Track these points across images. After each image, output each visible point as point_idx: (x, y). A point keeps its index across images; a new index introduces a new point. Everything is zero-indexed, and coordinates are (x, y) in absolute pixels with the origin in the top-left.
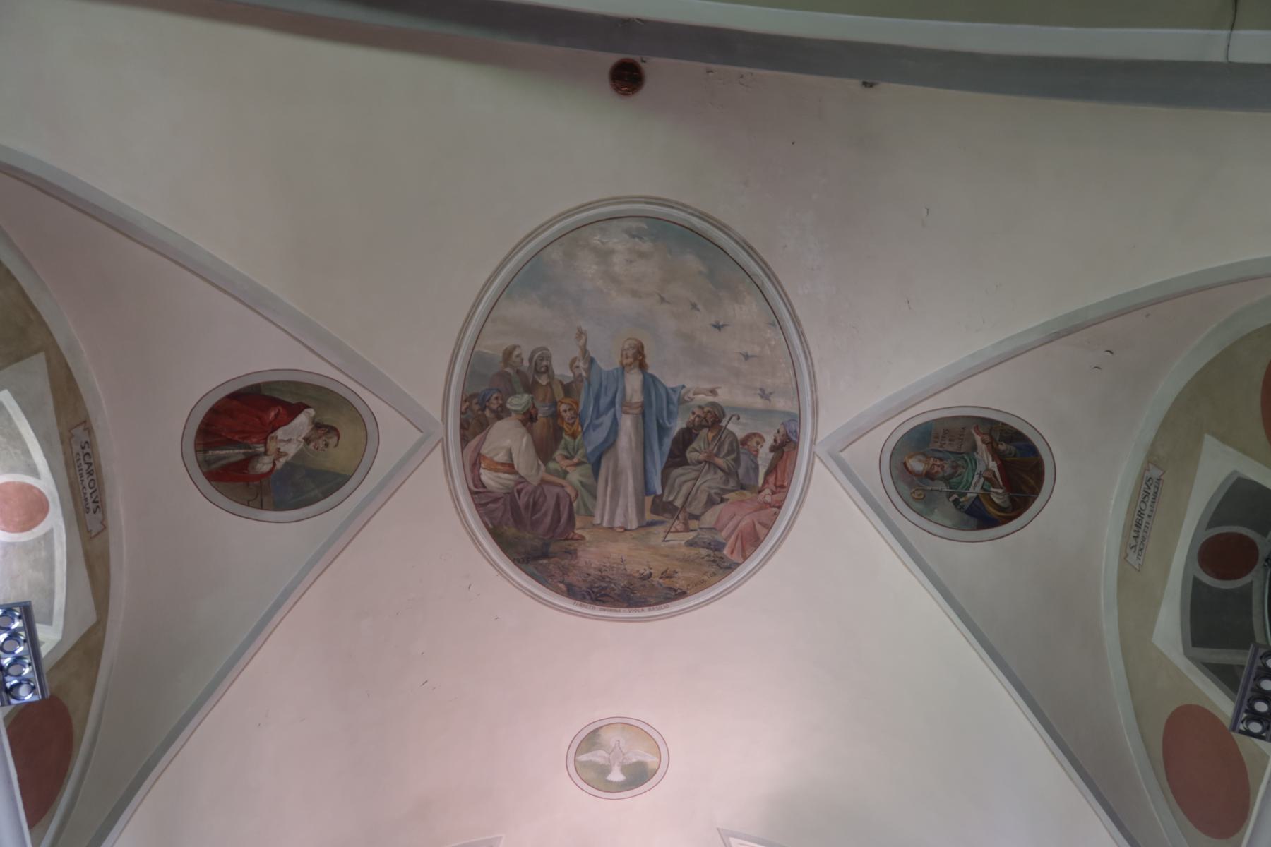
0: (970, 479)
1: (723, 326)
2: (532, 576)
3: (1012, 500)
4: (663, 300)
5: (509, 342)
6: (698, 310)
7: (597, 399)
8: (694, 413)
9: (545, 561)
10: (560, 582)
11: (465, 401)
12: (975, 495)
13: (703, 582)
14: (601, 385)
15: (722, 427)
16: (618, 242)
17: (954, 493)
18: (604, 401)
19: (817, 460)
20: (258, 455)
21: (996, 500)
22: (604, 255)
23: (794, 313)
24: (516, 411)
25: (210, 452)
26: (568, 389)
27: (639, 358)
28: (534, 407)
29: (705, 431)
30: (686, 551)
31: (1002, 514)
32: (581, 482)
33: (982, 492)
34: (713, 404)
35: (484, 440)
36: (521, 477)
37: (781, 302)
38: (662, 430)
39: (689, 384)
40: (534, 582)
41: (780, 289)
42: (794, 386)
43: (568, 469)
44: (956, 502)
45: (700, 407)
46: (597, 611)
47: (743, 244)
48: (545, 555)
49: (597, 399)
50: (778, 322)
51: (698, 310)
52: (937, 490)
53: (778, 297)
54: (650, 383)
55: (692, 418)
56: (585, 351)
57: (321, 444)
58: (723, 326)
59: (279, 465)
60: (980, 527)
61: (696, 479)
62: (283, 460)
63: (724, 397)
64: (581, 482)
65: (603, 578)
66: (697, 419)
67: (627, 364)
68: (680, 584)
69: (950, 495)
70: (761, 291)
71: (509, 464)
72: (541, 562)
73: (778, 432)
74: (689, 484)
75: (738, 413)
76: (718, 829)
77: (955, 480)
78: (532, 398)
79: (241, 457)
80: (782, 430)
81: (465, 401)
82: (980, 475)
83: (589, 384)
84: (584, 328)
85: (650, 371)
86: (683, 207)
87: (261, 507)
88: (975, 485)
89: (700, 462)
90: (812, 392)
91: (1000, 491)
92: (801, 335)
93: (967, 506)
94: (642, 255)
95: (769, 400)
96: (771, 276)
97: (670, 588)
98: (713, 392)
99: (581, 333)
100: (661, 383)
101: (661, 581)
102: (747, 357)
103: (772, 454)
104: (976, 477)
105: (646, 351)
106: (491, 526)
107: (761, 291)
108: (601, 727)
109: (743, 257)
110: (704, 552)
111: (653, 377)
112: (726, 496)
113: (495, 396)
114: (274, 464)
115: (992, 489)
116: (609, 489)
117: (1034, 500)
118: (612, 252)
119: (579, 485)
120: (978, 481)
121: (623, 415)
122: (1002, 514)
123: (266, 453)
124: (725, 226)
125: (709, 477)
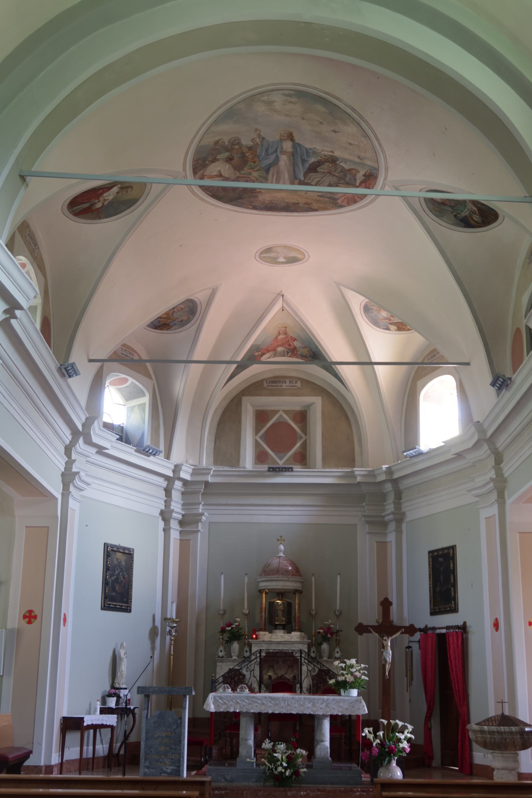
0: (463, 209)
1: (337, 132)
2: (234, 205)
3: (482, 220)
4: (303, 119)
5: (217, 138)
6: (324, 124)
7: (267, 150)
8: (321, 157)
9: (240, 200)
10: (249, 205)
11: (195, 161)
12: (465, 215)
13: (327, 208)
14: (269, 145)
15: (336, 164)
16: (278, 99)
17: (454, 212)
18: (270, 151)
19: (386, 185)
20: (96, 203)
21: (475, 219)
22: (269, 103)
23: (377, 136)
24: (222, 159)
25: (74, 208)
26: (250, 148)
27: (291, 137)
28: (232, 156)
29: (328, 164)
30: (318, 198)
31: (477, 224)
32: (259, 176)
33: (469, 215)
34: (332, 156)
35: (206, 170)
36: (226, 177)
37: (369, 130)
38: (304, 161)
39: (318, 148)
40: (237, 207)
41: (369, 126)
42: (376, 159)
43: (252, 172)
44: (455, 216)
45: (325, 156)
46: (270, 213)
47: (349, 107)
48: (240, 198)
49: (267, 150)
50: (366, 135)
51: (324, 124)
52: (446, 209)
53: (367, 128)
54: (296, 146)
55: (320, 158)
56: (259, 135)
57: (124, 192)
58: (337, 132)
59: (106, 203)
60: (465, 227)
61: (323, 177)
62: (107, 202)
63: (337, 154)
64: (259, 176)
65: (273, 204)
66: (323, 159)
67: (283, 139)
68: (315, 206)
69: (452, 212)
70: (359, 125)
71: (220, 175)
72: (239, 201)
73: (367, 171)
74: (320, 178)
75: (346, 161)
76: (335, 282)
77: (455, 208)
78: (231, 153)
79: (89, 205)
80: (369, 171)
81: (195, 161)
82: (468, 209)
83: (262, 146)
84: (258, 128)
85: (297, 141)
86: (316, 89)
87: (100, 218)
88: (465, 212)
89: (325, 173)
90: (385, 164)
91: (477, 217)
92: (380, 145)
93: (460, 218)
94: (291, 102)
95: (363, 160)
96: (365, 121)
97: (309, 208)
98: (332, 152)
99: (256, 130)
100: (304, 147)
101: (304, 205)
102: (350, 144)
103: (363, 177)
104: (466, 210)
105: (294, 135)
106: (211, 194)
107: (359, 125)
108: (273, 247)
109: (349, 111)
110: (327, 199)
111: (299, 144)
112: (338, 185)
113: (210, 156)
114: (103, 204)
115: (473, 215)
116: (275, 177)
117: (493, 223)
118: (274, 101)
119: (258, 176)
120: (467, 211)
121: (282, 155)
122: (477, 224)
123: (99, 202)
124: (339, 98)
125: (330, 177)
